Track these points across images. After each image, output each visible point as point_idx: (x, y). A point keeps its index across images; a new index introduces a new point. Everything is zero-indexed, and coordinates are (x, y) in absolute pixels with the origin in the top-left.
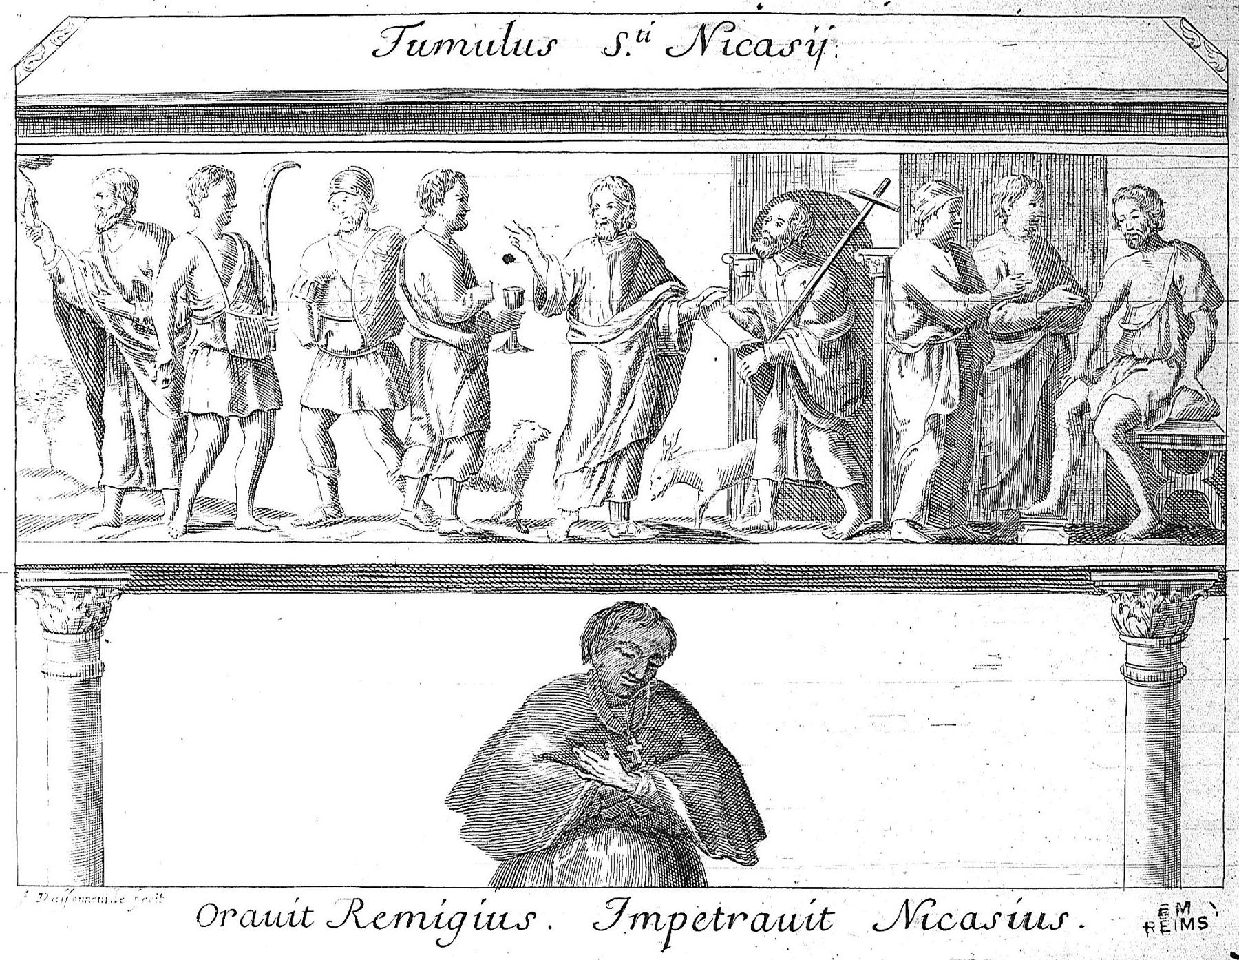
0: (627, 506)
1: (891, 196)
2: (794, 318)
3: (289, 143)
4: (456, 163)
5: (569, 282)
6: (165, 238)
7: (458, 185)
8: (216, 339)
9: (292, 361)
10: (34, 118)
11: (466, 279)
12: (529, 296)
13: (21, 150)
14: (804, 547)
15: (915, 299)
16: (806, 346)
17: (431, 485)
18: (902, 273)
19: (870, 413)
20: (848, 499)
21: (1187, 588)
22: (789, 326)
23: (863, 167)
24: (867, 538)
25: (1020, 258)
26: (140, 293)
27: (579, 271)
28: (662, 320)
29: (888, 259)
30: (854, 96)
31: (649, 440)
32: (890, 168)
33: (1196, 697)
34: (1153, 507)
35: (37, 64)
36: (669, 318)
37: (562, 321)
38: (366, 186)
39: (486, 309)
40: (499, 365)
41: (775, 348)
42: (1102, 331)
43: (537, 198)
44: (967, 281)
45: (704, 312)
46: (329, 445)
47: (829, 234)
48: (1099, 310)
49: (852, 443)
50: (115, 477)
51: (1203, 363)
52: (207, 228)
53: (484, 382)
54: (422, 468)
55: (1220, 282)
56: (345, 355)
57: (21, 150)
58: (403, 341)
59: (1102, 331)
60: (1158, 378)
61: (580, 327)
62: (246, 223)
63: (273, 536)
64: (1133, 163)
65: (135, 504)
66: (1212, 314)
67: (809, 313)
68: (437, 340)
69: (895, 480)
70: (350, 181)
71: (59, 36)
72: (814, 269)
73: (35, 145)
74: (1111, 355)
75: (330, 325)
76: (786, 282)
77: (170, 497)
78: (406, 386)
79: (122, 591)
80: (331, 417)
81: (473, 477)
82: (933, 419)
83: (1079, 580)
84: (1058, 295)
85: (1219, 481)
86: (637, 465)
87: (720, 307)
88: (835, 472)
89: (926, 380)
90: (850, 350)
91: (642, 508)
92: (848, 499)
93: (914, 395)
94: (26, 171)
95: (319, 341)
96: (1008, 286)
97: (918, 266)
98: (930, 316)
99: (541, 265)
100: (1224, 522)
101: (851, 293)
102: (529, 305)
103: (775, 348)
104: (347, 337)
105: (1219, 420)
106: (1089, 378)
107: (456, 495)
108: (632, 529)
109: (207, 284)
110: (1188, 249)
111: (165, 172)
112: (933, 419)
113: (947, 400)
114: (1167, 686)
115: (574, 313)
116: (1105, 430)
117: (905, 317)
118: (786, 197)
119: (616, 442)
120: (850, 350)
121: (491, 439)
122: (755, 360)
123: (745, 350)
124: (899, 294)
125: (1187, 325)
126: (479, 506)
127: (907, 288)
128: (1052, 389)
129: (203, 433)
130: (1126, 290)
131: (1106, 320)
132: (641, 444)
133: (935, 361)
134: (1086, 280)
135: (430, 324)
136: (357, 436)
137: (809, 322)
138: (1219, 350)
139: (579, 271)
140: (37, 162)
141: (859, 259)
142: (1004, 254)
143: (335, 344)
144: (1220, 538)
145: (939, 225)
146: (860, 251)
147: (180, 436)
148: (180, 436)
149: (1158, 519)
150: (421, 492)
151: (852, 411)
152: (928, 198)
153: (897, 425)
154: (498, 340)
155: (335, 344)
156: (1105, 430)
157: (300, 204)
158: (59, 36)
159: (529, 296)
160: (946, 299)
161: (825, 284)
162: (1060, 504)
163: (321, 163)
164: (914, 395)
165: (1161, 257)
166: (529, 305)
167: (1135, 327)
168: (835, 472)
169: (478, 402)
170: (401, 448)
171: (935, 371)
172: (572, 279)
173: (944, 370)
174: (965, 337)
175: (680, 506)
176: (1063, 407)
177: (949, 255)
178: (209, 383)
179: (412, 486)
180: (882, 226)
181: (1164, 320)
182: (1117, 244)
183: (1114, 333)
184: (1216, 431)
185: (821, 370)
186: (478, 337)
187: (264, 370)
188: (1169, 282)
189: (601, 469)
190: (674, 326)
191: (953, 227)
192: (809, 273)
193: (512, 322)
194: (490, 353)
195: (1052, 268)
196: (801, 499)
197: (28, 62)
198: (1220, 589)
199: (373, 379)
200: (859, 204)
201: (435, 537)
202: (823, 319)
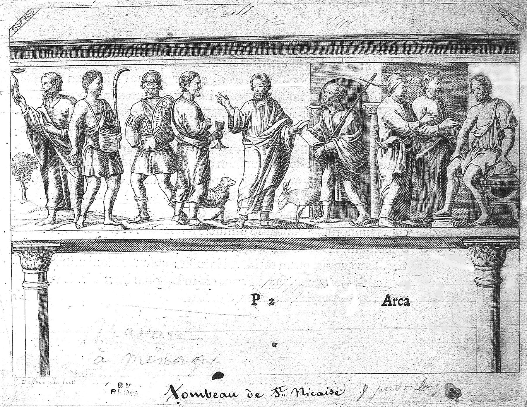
0: (268, 213)
1: (378, 80)
2: (337, 134)
3: (122, 61)
4: (196, 69)
5: (243, 118)
6: (74, 102)
7: (196, 79)
8: (94, 144)
9: (127, 155)
10: (22, 50)
11: (200, 117)
12: (226, 126)
13: (12, 65)
14: (342, 228)
15: (388, 125)
16: (342, 145)
17: (186, 205)
18: (381, 113)
19: (369, 173)
20: (360, 209)
21: (502, 246)
22: (335, 136)
23: (366, 67)
24: (369, 225)
25: (433, 107)
26: (64, 124)
27: (247, 113)
28: (282, 135)
29: (376, 108)
30: (359, 38)
31: (277, 186)
32: (377, 69)
33: (509, 286)
34: (487, 211)
35: (18, 28)
36: (285, 134)
37: (240, 136)
38: (158, 80)
39: (209, 130)
40: (214, 155)
41: (330, 145)
42: (466, 136)
43: (226, 84)
44: (411, 117)
45: (299, 131)
46: (143, 189)
47: (351, 96)
48: (466, 125)
49: (361, 186)
50: (52, 204)
51: (508, 151)
52: (91, 99)
53: (208, 161)
54: (182, 199)
55: (516, 114)
56: (149, 151)
57: (12, 65)
58: (174, 144)
59: (466, 136)
60: (489, 157)
61: (249, 138)
62: (107, 94)
63: (119, 227)
64: (478, 66)
65: (61, 214)
66: (513, 129)
67: (343, 131)
68: (189, 144)
69: (381, 201)
70: (150, 78)
71: (28, 16)
72: (344, 112)
73: (21, 63)
74: (470, 148)
75: (143, 138)
76: (336, 117)
77: (76, 211)
78: (176, 164)
79: (56, 251)
80: (144, 177)
81: (204, 201)
82: (395, 175)
83: (459, 243)
84: (448, 123)
85: (517, 200)
86: (273, 195)
87: (306, 128)
88: (354, 197)
89: (393, 158)
90: (360, 147)
91: (275, 214)
92: (360, 209)
93: (387, 165)
94: (14, 74)
95: (138, 145)
96: (427, 118)
97: (389, 111)
98: (396, 132)
99: (231, 112)
100: (519, 218)
101: (362, 120)
102: (226, 129)
103: (330, 145)
104: (150, 143)
105: (516, 174)
106: (462, 155)
107: (196, 209)
108: (270, 224)
109: (91, 123)
110: (499, 102)
111: (73, 72)
112: (395, 175)
113: (401, 166)
114: (496, 285)
115: (246, 133)
116: (467, 180)
117: (383, 132)
118: (334, 81)
119: (263, 186)
120: (360, 147)
121: (211, 185)
122: (319, 151)
123: (316, 147)
124: (381, 124)
125: (502, 135)
126: (207, 213)
127: (384, 119)
128: (446, 162)
129: (90, 186)
130: (475, 120)
131: (468, 132)
132: (275, 187)
133: (396, 150)
134: (460, 117)
135: (186, 138)
136: (155, 186)
137: (343, 134)
138: (516, 145)
139: (247, 113)
140: (18, 70)
141: (364, 108)
142: (425, 105)
143: (146, 146)
144: (515, 224)
145: (399, 91)
146: (364, 104)
147: (80, 187)
148: (80, 187)
149: (490, 216)
150: (182, 207)
151: (361, 173)
152: (394, 80)
153: (380, 177)
154: (214, 143)
155: (146, 146)
156: (467, 180)
157: (127, 88)
158: (28, 16)
159: (226, 126)
160: (400, 124)
161: (350, 119)
162: (450, 208)
163: (139, 68)
164: (387, 165)
165: (489, 106)
166: (226, 129)
167: (480, 135)
168: (354, 197)
169: (205, 169)
170: (174, 191)
171: (396, 156)
172: (244, 117)
173: (400, 153)
174: (404, 142)
175: (289, 213)
176: (451, 169)
177: (402, 105)
178: (92, 163)
179: (178, 206)
180: (374, 93)
181: (491, 133)
182: (472, 100)
183: (471, 137)
184: (515, 179)
185: (347, 154)
186: (205, 141)
187: (115, 157)
188: (494, 116)
189: (257, 197)
190: (287, 136)
191: (403, 95)
192: (343, 113)
193: (219, 135)
194: (210, 149)
195: (445, 112)
196: (341, 209)
197: (15, 28)
198: (517, 246)
199: (161, 161)
200: (364, 84)
201: (187, 227)
202: (349, 133)
